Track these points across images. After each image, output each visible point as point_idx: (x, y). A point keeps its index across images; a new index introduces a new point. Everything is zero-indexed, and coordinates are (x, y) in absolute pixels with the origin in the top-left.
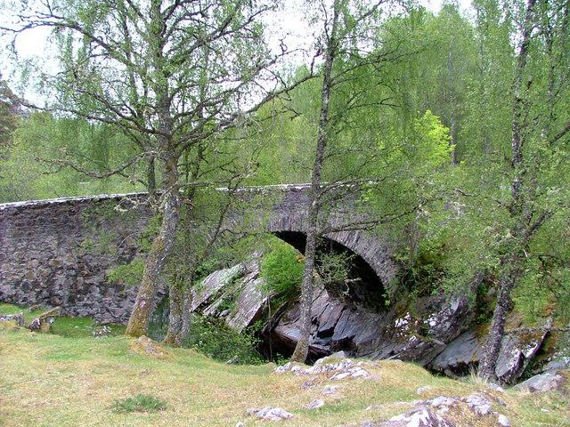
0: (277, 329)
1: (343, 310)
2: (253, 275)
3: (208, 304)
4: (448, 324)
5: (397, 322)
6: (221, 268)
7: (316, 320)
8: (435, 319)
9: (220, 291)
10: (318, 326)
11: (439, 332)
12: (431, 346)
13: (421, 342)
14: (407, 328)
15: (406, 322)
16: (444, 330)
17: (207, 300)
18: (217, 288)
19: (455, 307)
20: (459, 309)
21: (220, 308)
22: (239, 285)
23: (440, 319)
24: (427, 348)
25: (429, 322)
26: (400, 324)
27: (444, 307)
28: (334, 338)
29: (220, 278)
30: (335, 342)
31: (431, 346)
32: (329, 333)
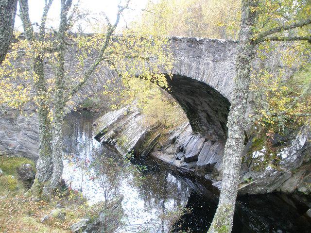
0: (153, 154)
1: (205, 141)
2: (134, 114)
3: (104, 134)
4: (295, 157)
5: (254, 153)
6: (213, 40)
7: (182, 148)
8: (287, 152)
9: (111, 125)
10: (184, 153)
11: (288, 163)
12: (282, 174)
13: (274, 171)
14: (263, 159)
15: (262, 154)
16: (292, 161)
17: (102, 131)
18: (109, 124)
19: (302, 143)
20: (305, 145)
21: (113, 137)
22: (122, 123)
23: (290, 153)
24: (279, 176)
25: (281, 155)
26: (256, 156)
27: (293, 142)
28: (198, 164)
29: (25, 126)
30: (199, 167)
31: (282, 174)
32: (194, 159)
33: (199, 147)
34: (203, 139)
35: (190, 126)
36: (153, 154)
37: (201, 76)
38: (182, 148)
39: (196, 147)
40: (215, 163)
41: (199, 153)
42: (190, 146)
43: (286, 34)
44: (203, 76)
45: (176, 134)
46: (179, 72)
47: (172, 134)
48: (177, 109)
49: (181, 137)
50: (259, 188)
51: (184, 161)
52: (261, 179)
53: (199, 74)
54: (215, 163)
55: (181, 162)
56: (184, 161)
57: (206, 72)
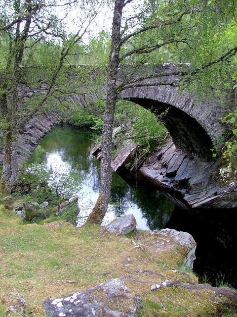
0: (141, 169)
1: (185, 158)
7: (166, 165)
10: (167, 169)
30: (177, 181)
33: (179, 163)
34: (183, 156)
35: (174, 145)
36: (141, 169)
37: (167, 98)
38: (166, 165)
39: (177, 163)
40: (189, 179)
41: (178, 169)
42: (172, 162)
43: (152, 48)
44: (170, 98)
45: (162, 151)
46: (145, 95)
47: (160, 150)
48: (198, 119)
49: (166, 154)
50: (224, 202)
51: (166, 176)
52: (225, 194)
53: (165, 97)
54: (189, 179)
55: (163, 177)
56: (166, 176)
57: (173, 94)
